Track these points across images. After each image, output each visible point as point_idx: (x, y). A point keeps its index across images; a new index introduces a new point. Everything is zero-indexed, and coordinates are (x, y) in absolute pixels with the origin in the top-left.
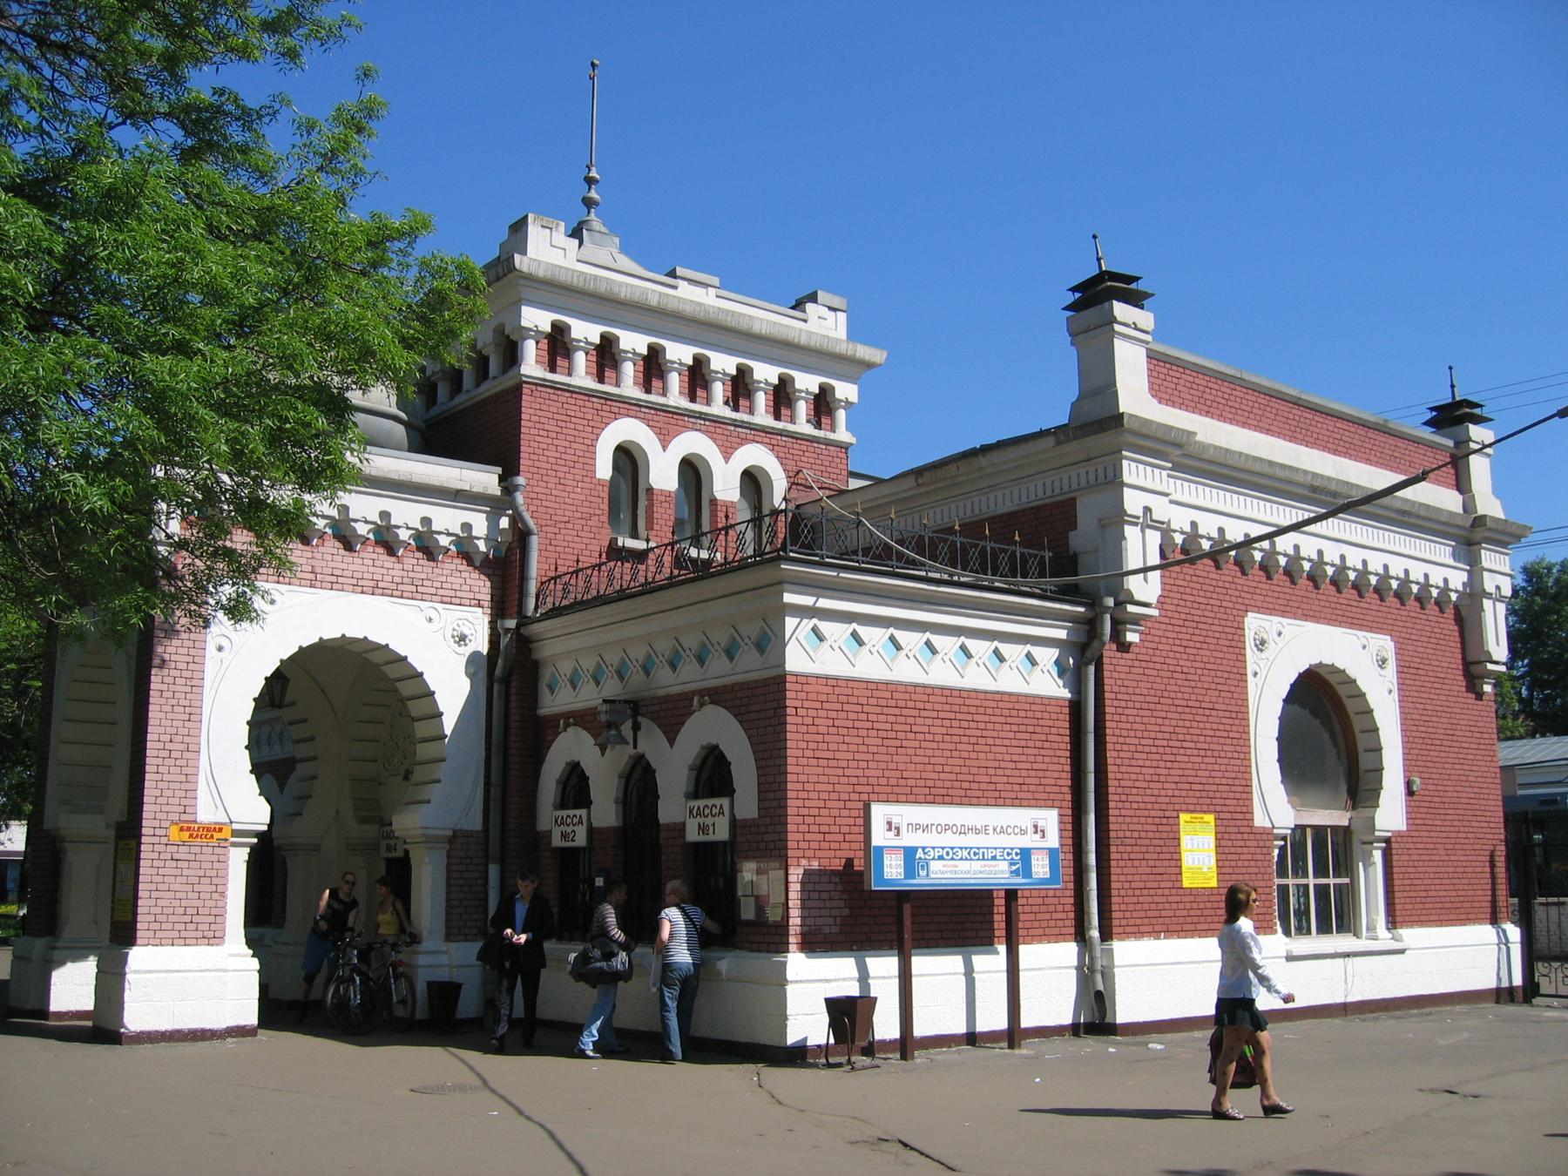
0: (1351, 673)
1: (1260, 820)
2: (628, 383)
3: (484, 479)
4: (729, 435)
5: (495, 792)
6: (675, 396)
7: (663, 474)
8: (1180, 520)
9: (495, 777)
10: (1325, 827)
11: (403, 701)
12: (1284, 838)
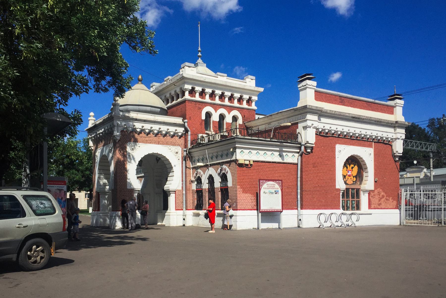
0: (361, 156)
1: (337, 187)
2: (207, 99)
3: (179, 120)
4: (230, 109)
5: (184, 182)
7: (215, 118)
10: (349, 189)
11: (165, 165)
12: (139, 191)
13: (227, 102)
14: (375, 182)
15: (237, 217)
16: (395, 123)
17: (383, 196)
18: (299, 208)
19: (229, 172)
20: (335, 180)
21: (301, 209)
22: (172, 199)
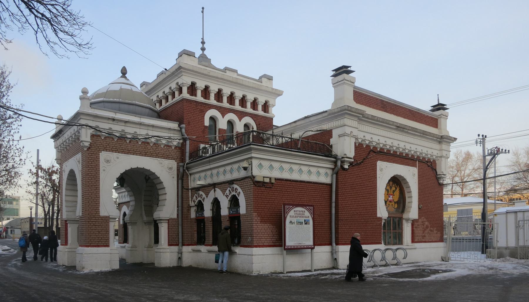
1: (379, 215)
2: (212, 101)
3: (174, 125)
4: (241, 115)
5: (180, 208)
6: (225, 104)
8: (361, 135)
9: (180, 204)
13: (237, 106)
14: (419, 208)
15: (253, 256)
16: (440, 137)
17: (427, 227)
18: (334, 244)
19: (242, 194)
20: (376, 206)
21: (337, 244)
22: (164, 230)
